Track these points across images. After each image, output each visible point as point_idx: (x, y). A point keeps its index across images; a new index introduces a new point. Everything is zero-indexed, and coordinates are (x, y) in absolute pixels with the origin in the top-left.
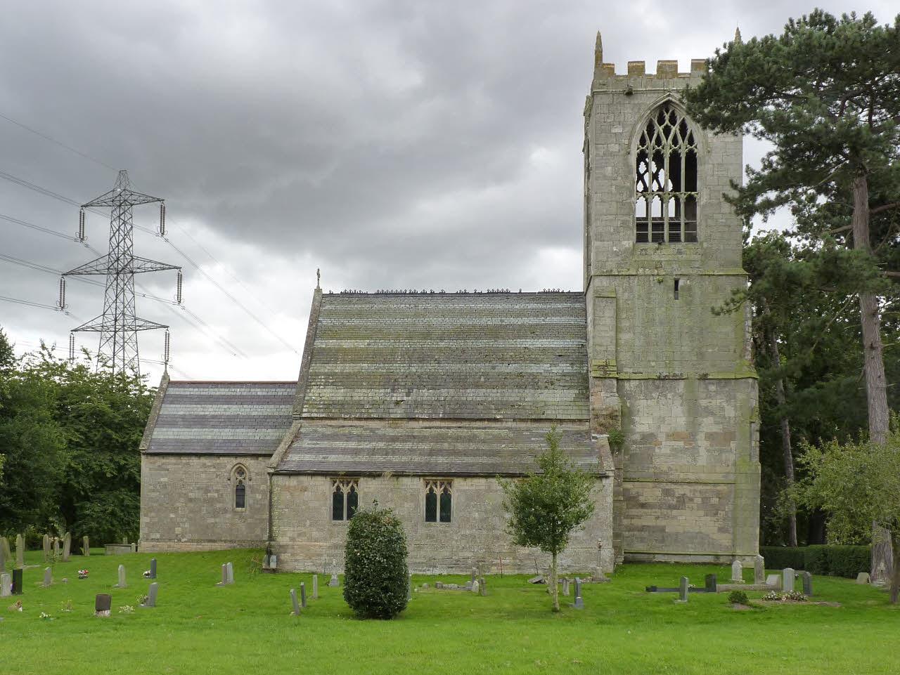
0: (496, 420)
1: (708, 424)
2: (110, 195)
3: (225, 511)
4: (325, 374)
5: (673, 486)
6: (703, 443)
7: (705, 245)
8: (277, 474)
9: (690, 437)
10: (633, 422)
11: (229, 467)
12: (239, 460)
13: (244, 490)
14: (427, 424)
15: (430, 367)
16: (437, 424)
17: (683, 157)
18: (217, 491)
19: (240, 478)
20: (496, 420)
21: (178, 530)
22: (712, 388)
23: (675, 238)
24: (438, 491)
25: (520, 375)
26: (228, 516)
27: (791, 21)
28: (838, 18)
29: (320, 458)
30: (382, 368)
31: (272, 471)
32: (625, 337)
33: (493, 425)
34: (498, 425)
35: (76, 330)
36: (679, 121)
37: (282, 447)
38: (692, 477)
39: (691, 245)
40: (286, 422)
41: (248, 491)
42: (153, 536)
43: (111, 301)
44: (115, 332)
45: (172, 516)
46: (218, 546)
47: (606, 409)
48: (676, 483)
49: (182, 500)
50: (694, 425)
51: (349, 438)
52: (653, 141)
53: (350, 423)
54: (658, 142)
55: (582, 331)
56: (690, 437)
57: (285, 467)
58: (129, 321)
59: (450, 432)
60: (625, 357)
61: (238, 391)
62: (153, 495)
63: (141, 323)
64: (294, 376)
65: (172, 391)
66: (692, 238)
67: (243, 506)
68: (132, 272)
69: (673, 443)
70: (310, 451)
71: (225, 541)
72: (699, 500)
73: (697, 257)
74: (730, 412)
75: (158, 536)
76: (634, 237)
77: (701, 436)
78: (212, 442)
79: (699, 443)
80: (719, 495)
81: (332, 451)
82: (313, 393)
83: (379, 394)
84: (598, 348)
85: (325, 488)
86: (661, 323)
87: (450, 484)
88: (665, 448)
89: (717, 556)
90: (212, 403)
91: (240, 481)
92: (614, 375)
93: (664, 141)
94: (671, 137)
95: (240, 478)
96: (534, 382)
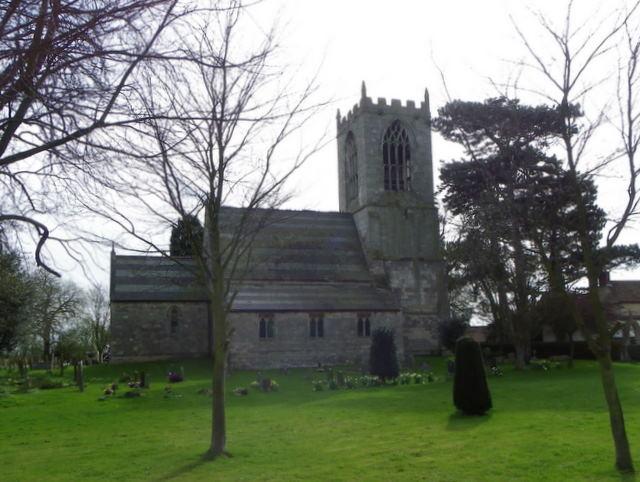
1: (424, 284)
6: (423, 293)
9: (416, 290)
20: (323, 281)
36: (401, 130)
46: (163, 358)
50: (418, 284)
74: (434, 278)
77: (422, 289)
85: (256, 319)
88: (405, 296)
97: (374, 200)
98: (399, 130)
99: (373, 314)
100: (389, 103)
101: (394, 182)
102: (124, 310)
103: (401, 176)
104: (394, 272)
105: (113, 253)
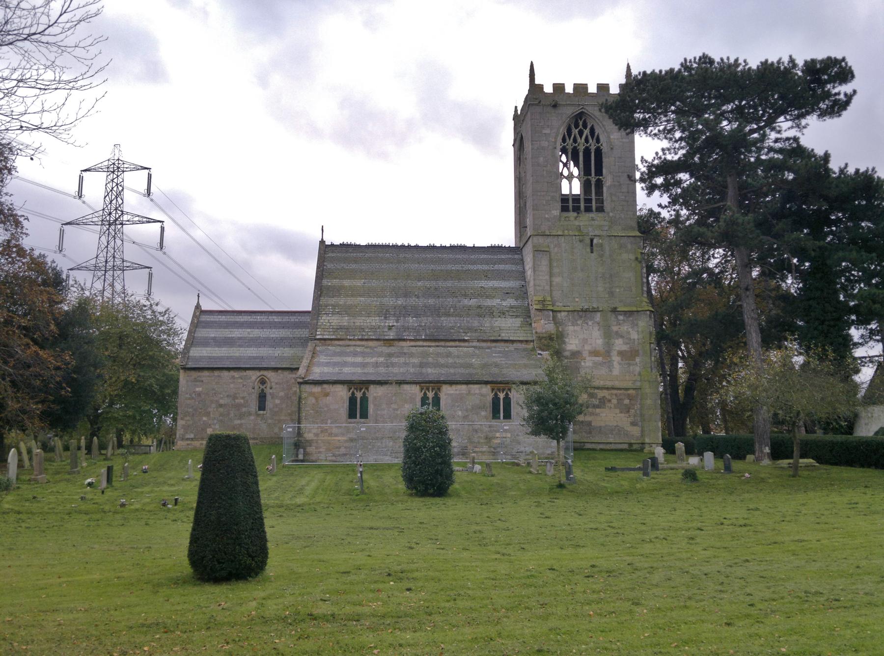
0: (464, 341)
2: (106, 163)
3: (250, 414)
4: (332, 305)
5: (596, 391)
6: (616, 359)
7: (611, 214)
8: (306, 383)
10: (564, 343)
11: (254, 378)
12: (262, 372)
14: (413, 343)
15: (412, 301)
16: (421, 343)
18: (243, 398)
19: (262, 387)
20: (464, 341)
22: (621, 318)
23: (588, 209)
25: (479, 307)
26: (252, 418)
27: (685, 60)
28: (717, 59)
29: (337, 370)
30: (375, 302)
31: (301, 380)
32: (557, 280)
33: (462, 344)
34: (466, 344)
35: (71, 269)
36: (589, 127)
37: (305, 362)
38: (609, 384)
39: (600, 215)
40: (304, 342)
41: (269, 397)
42: (188, 436)
43: (103, 246)
44: (106, 271)
45: (205, 419)
47: (546, 333)
48: (598, 388)
50: (609, 346)
51: (355, 354)
53: (353, 343)
54: (575, 141)
55: (522, 275)
56: (607, 353)
57: (311, 378)
58: (118, 262)
59: (431, 349)
60: (557, 294)
61: (259, 318)
62: (189, 402)
63: (128, 264)
64: (309, 307)
65: (204, 318)
66: (600, 209)
67: (264, 410)
68: (122, 224)
69: (594, 358)
70: (327, 364)
72: (614, 401)
73: (606, 223)
75: (192, 436)
76: (559, 208)
77: (614, 353)
78: (221, 358)
79: (614, 358)
80: (630, 397)
81: (345, 364)
82: (324, 319)
83: (374, 321)
84: (538, 288)
85: (342, 393)
86: (582, 270)
87: (439, 389)
89: (631, 444)
90: (238, 328)
91: (263, 390)
92: (550, 307)
93: (591, 141)
94: (584, 137)
95: (262, 387)
96: (490, 312)
98: (585, 126)
104: (571, 328)
105: (198, 307)
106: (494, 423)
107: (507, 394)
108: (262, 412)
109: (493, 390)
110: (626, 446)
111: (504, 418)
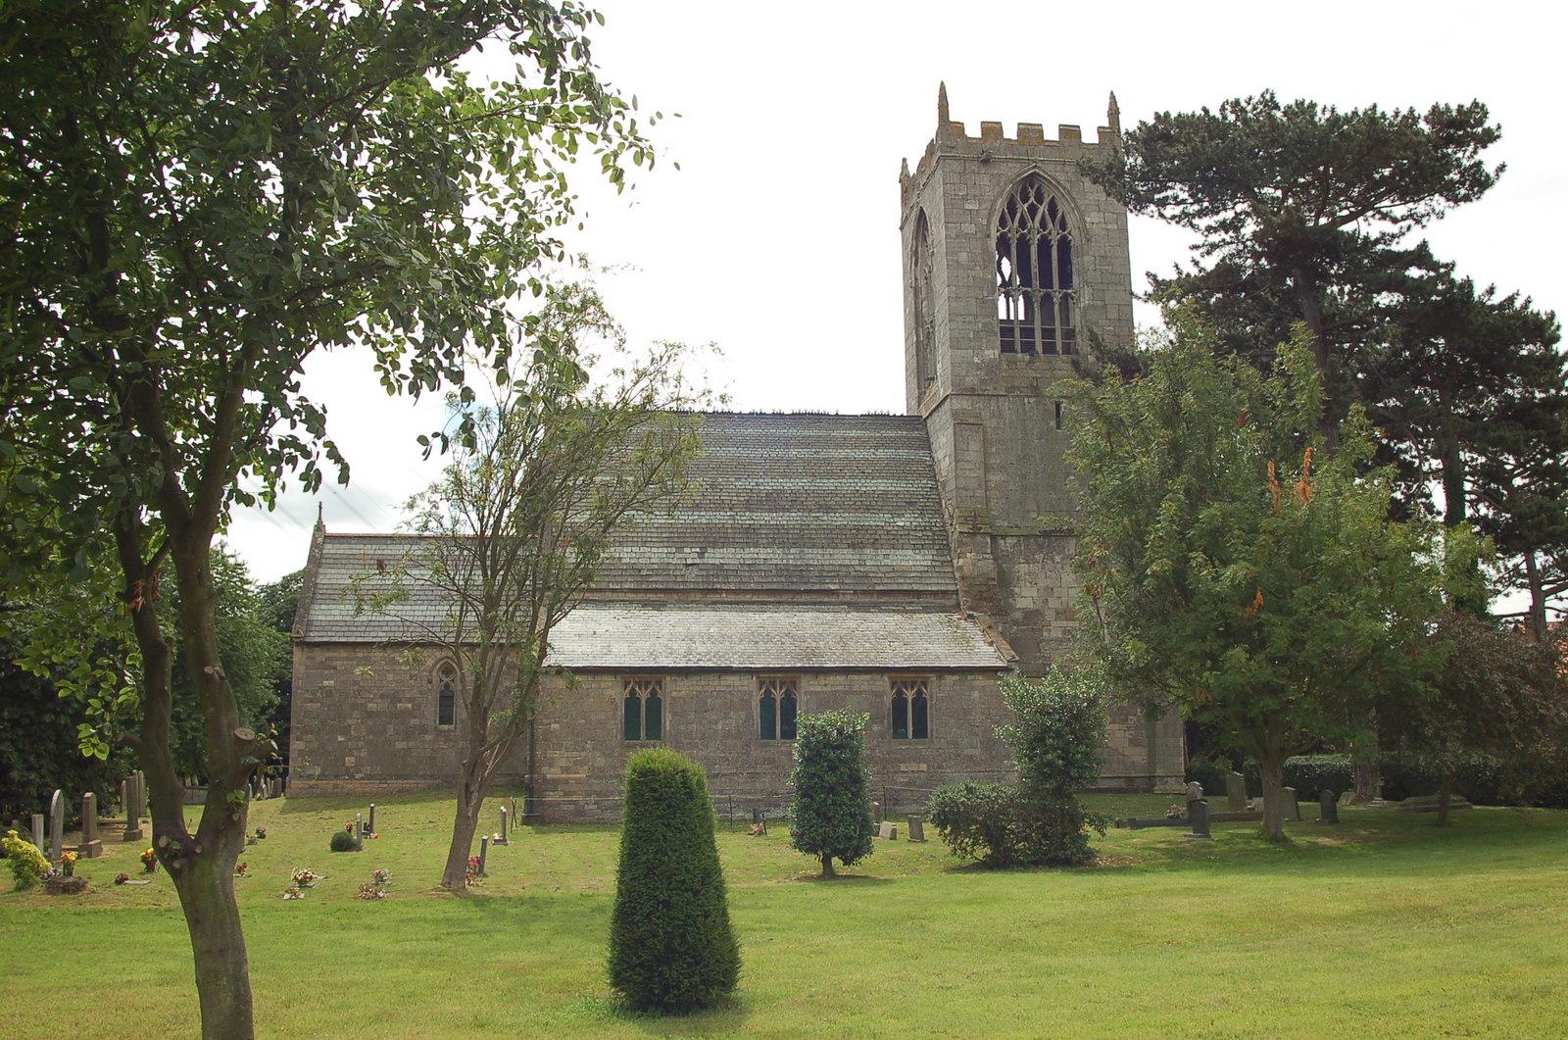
3: (423, 730)
10: (1012, 594)
11: (430, 662)
13: (452, 697)
17: (1054, 243)
18: (410, 700)
21: (349, 761)
24: (644, 695)
26: (429, 737)
34: (833, 599)
47: (979, 576)
49: (356, 714)
52: (1016, 223)
65: (329, 549)
71: (424, 777)
87: (794, 684)
89: (1129, 779)
91: (447, 685)
97: (971, 380)
98: (1039, 199)
99: (933, 677)
100: (1010, 133)
101: (1048, 333)
102: (323, 665)
103: (1066, 320)
104: (1023, 568)
105: (319, 527)
106: (901, 746)
107: (919, 693)
108: (446, 727)
109: (893, 684)
110: (1121, 784)
111: (915, 735)
